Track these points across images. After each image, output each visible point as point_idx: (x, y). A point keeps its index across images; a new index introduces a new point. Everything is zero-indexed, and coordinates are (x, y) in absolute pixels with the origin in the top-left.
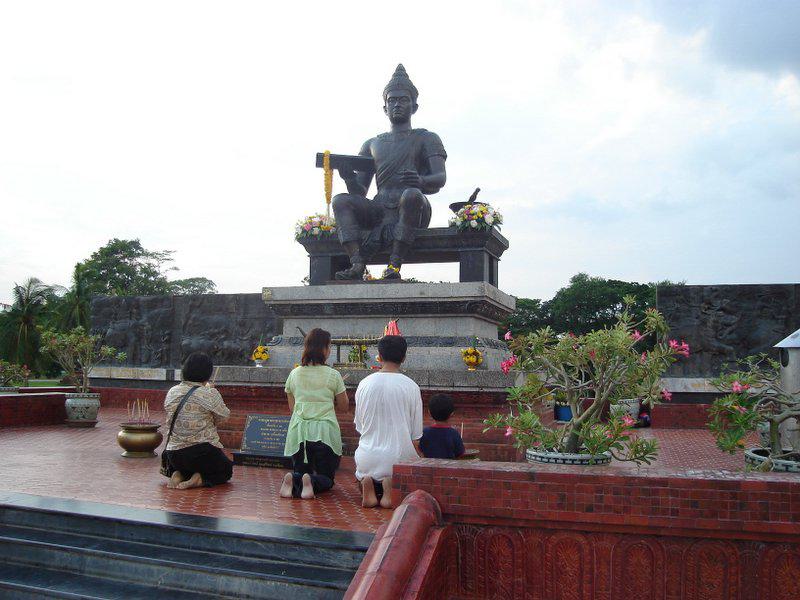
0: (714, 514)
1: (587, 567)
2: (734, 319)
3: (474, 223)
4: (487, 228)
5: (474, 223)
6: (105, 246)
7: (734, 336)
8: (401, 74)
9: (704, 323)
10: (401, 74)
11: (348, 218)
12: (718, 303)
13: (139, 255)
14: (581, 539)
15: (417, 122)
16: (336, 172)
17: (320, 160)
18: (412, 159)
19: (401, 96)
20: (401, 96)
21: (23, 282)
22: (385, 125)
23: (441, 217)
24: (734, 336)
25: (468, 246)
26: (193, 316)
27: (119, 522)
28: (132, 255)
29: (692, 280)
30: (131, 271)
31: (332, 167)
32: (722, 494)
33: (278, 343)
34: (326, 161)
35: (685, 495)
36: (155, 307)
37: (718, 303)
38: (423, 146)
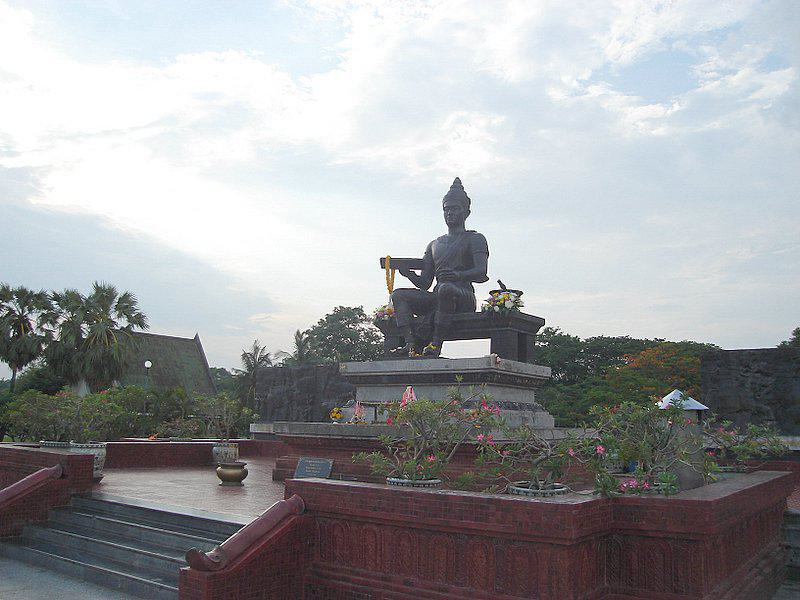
0: (435, 516)
1: (379, 547)
2: (770, 380)
3: (497, 309)
4: (507, 312)
5: (497, 309)
6: (331, 313)
7: (770, 396)
8: (457, 184)
9: (742, 385)
10: (457, 184)
11: (403, 307)
12: (755, 367)
13: (362, 321)
14: (375, 528)
15: (470, 224)
16: (397, 271)
17: (382, 260)
18: (462, 254)
19: (457, 204)
20: (457, 204)
21: (249, 350)
22: (445, 230)
23: (482, 294)
24: (770, 396)
25: (497, 326)
26: (330, 382)
27: (160, 512)
28: (355, 321)
29: (727, 344)
30: (355, 336)
31: (393, 269)
32: (440, 503)
33: (351, 405)
34: (387, 263)
35: (420, 502)
36: (302, 376)
37: (755, 367)
38: (469, 245)
